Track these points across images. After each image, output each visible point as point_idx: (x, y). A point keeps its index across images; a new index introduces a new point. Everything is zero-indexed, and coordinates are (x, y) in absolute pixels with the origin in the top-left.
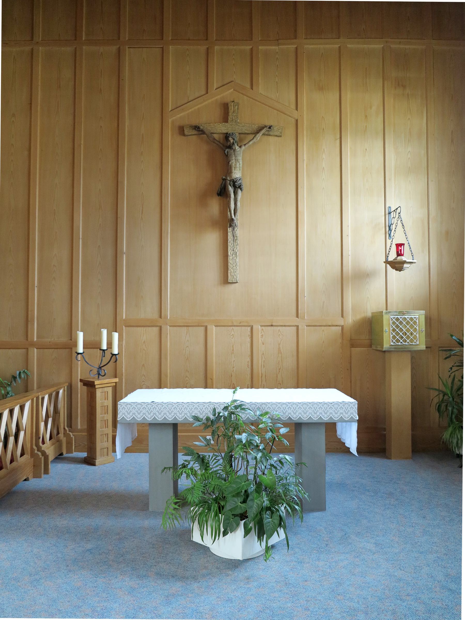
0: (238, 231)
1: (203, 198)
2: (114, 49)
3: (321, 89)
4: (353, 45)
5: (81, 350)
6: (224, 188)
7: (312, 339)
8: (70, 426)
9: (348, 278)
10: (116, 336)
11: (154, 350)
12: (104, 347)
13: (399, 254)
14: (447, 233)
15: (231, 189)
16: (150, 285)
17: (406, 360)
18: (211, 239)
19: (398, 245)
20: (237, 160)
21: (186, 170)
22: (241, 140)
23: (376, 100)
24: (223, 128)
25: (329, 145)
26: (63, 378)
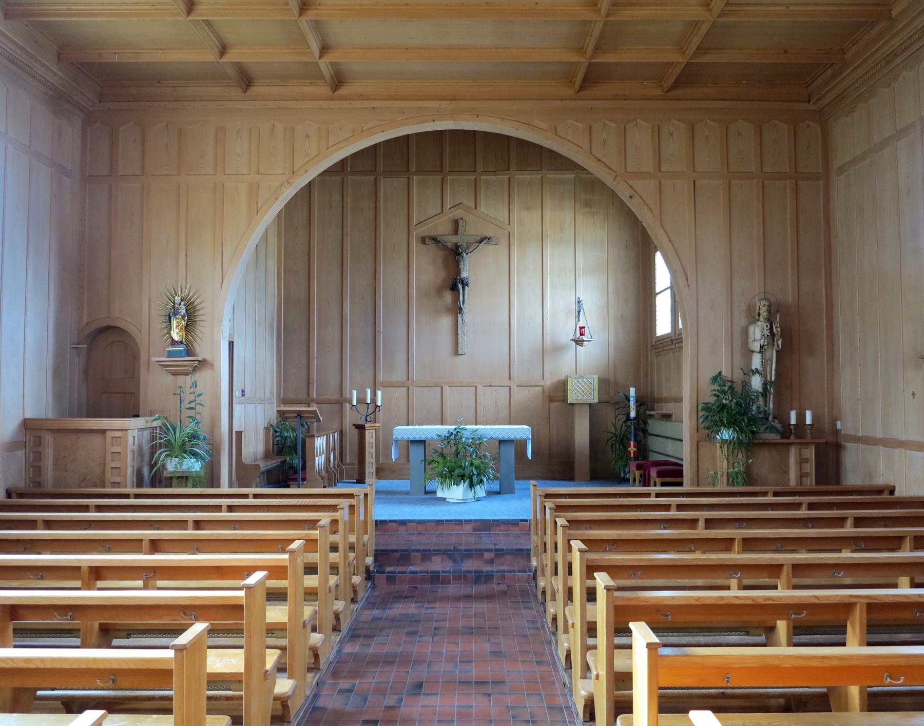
0: (466, 317)
1: (439, 291)
2: (372, 178)
3: (528, 208)
4: (552, 175)
5: (355, 403)
6: (455, 284)
7: (521, 396)
8: (342, 461)
9: (547, 351)
10: (379, 393)
11: (403, 404)
12: (369, 402)
13: (582, 334)
14: (622, 316)
15: (460, 286)
16: (401, 356)
17: (586, 410)
18: (446, 322)
19: (581, 328)
20: (464, 265)
21: (426, 269)
22: (468, 247)
23: (569, 216)
24: (452, 240)
25: (533, 253)
26: (336, 426)
